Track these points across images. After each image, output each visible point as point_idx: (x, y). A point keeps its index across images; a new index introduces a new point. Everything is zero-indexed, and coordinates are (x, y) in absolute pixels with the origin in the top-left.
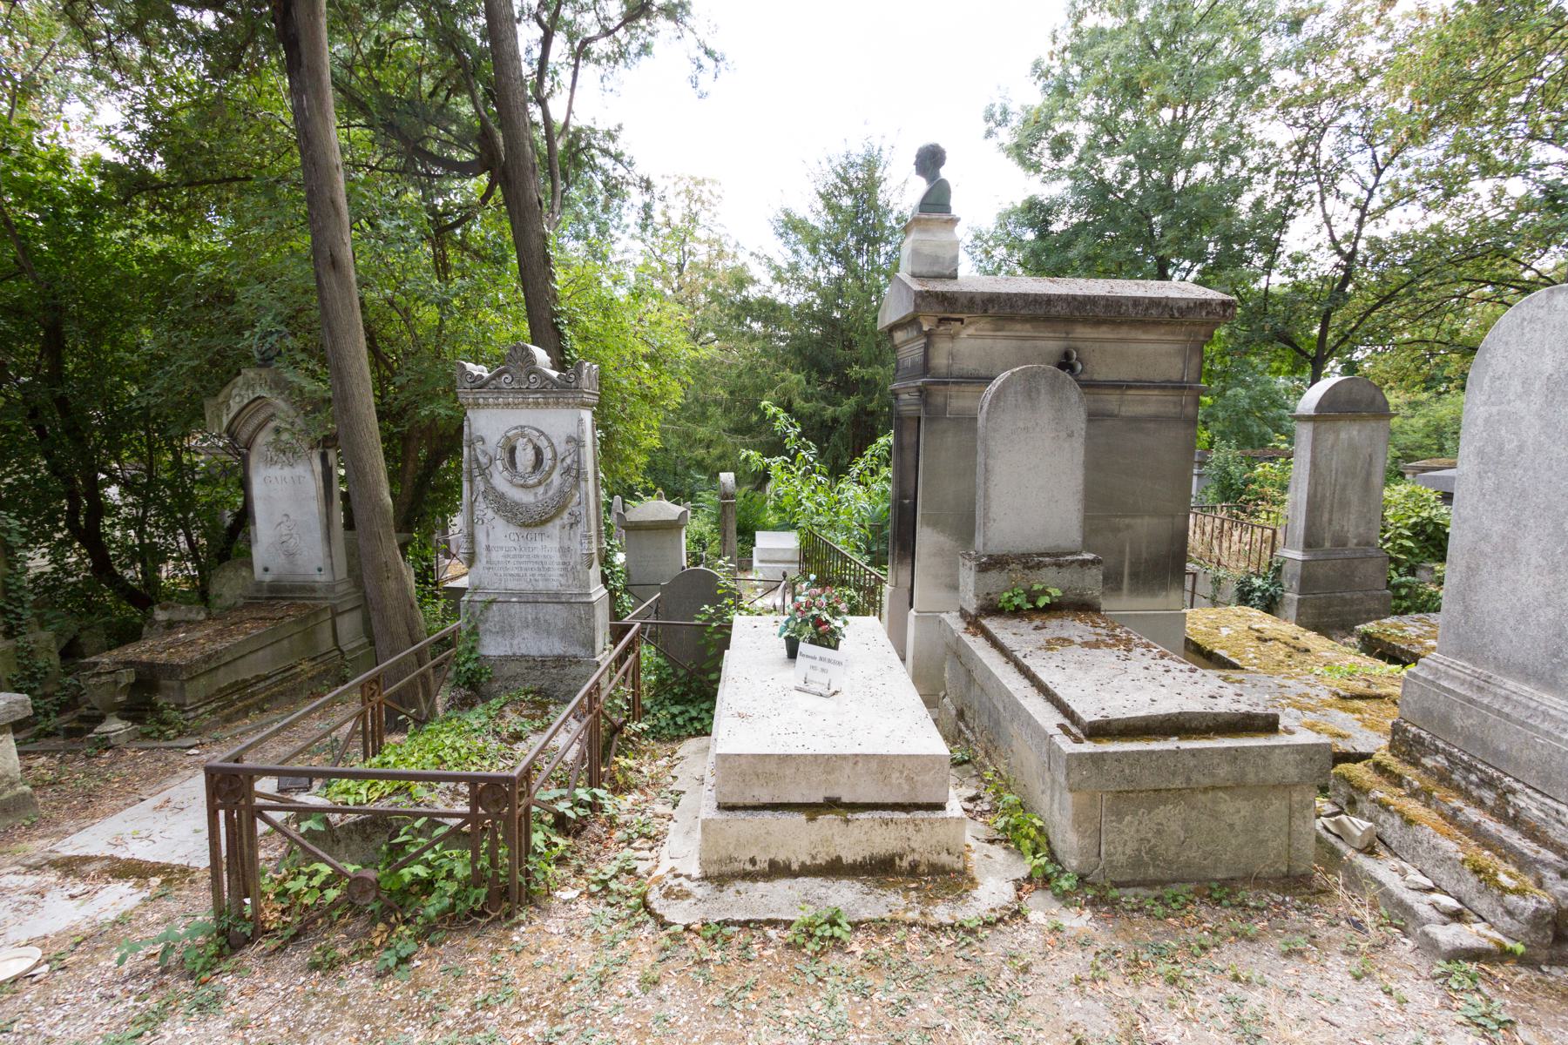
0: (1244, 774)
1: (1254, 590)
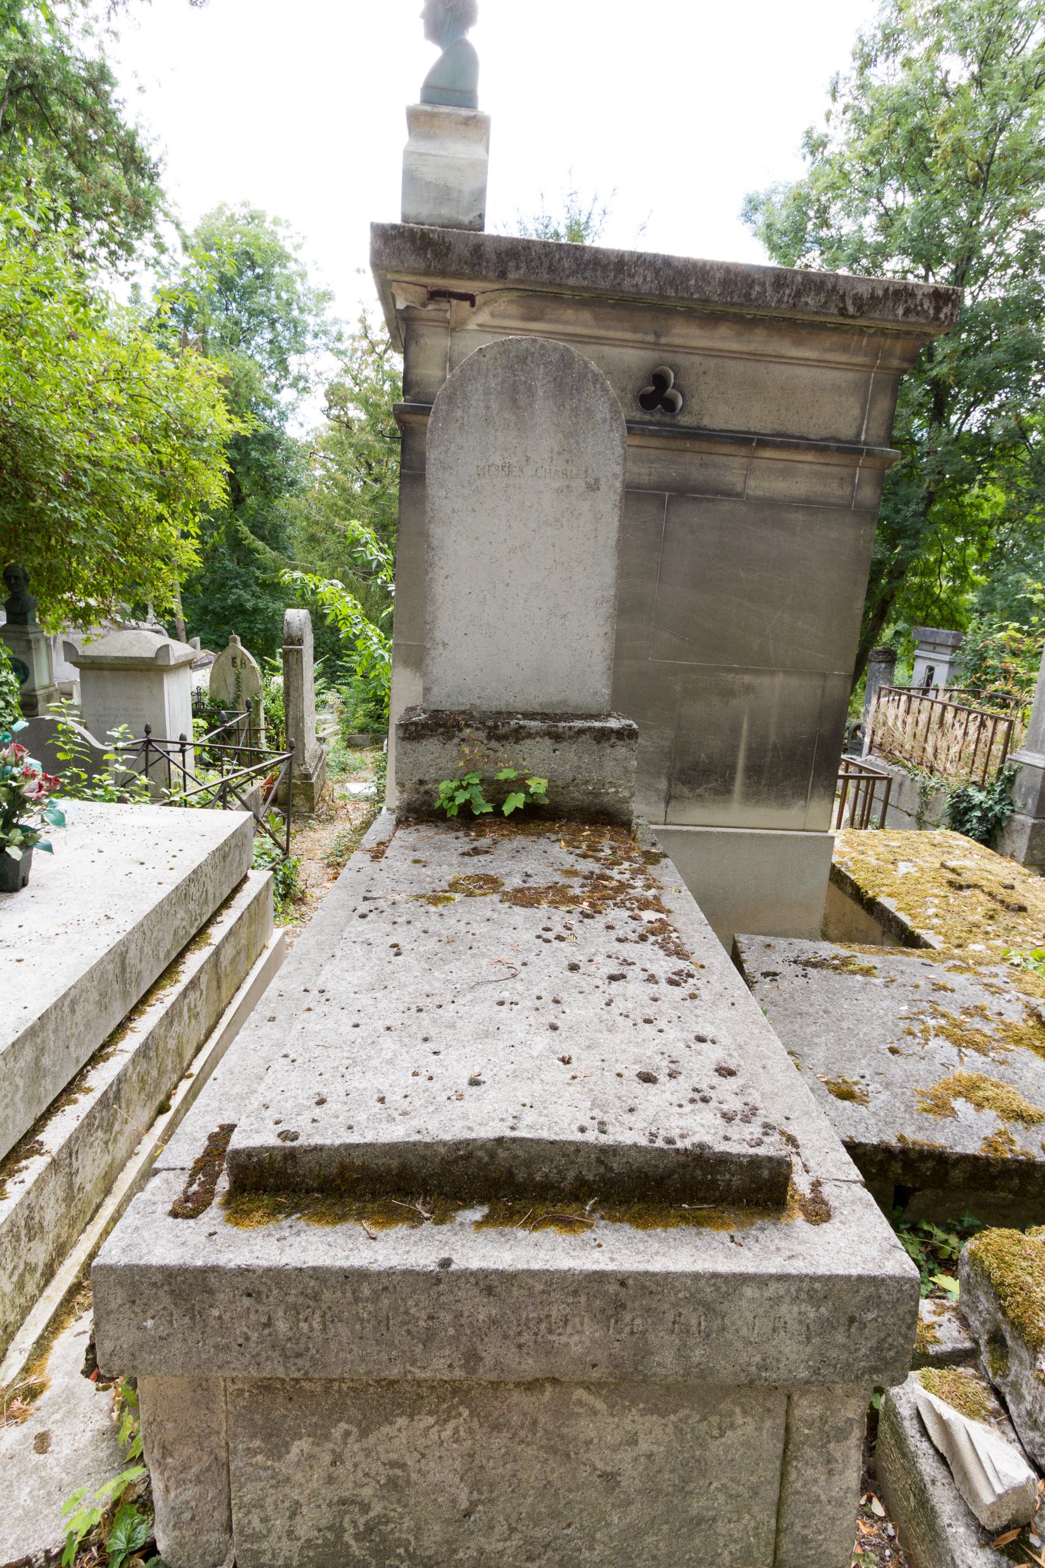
0: (644, 1352)
1: (973, 808)
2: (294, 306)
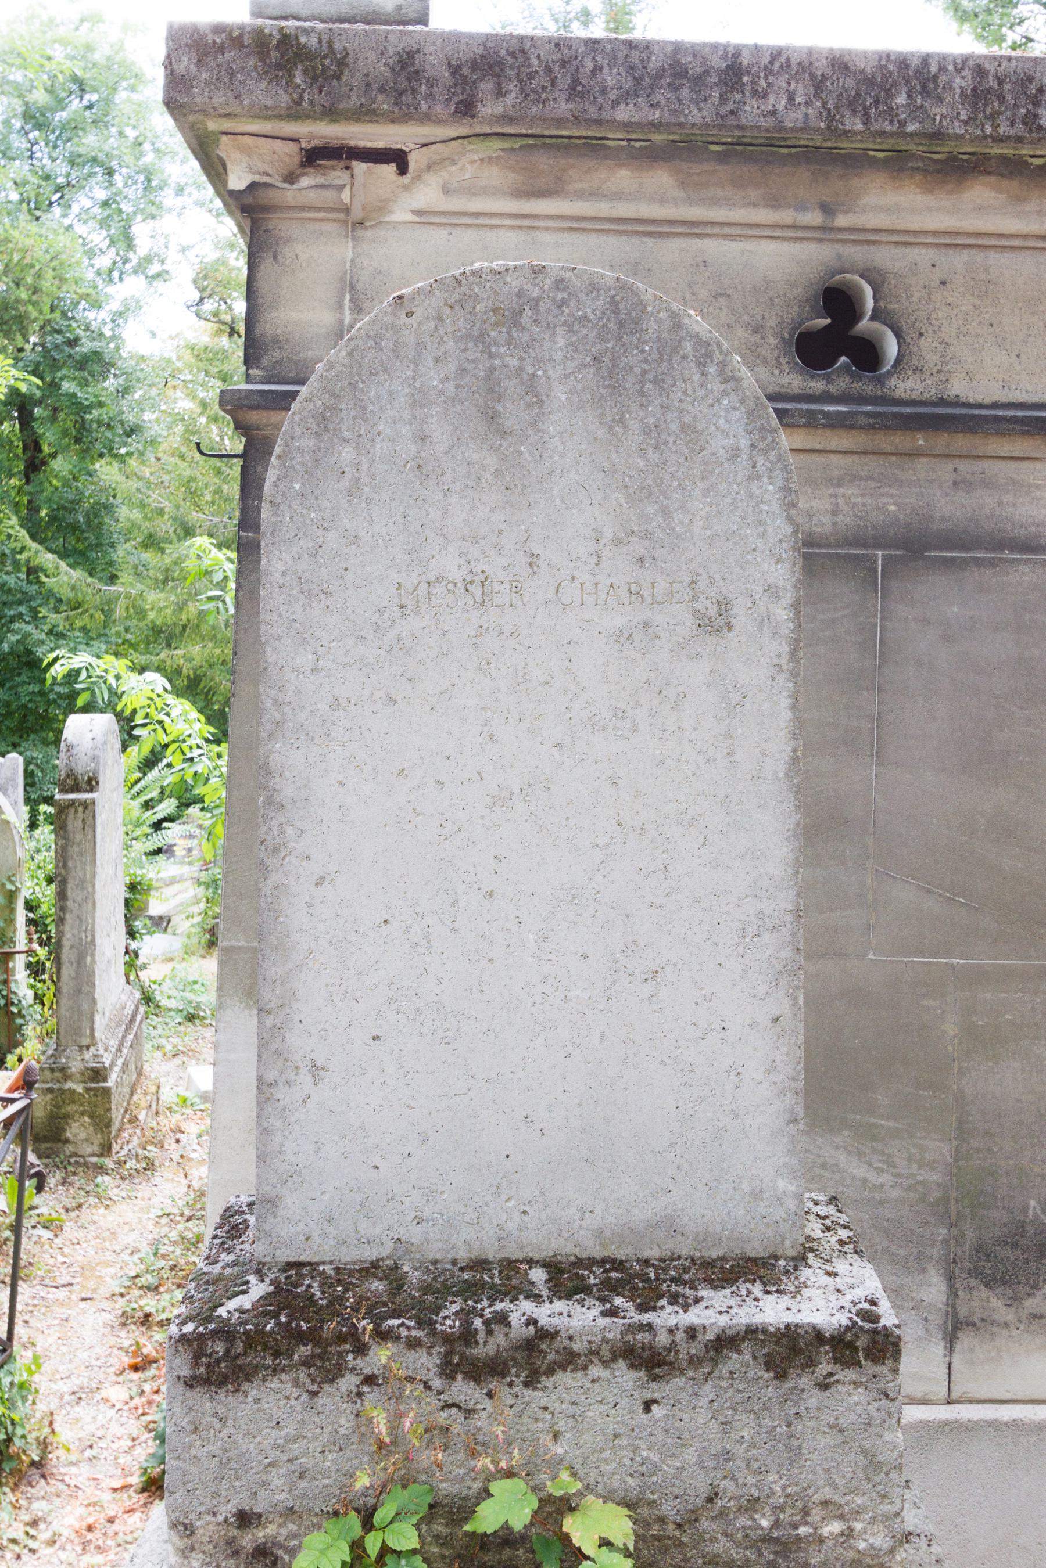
2: (147, 146)
